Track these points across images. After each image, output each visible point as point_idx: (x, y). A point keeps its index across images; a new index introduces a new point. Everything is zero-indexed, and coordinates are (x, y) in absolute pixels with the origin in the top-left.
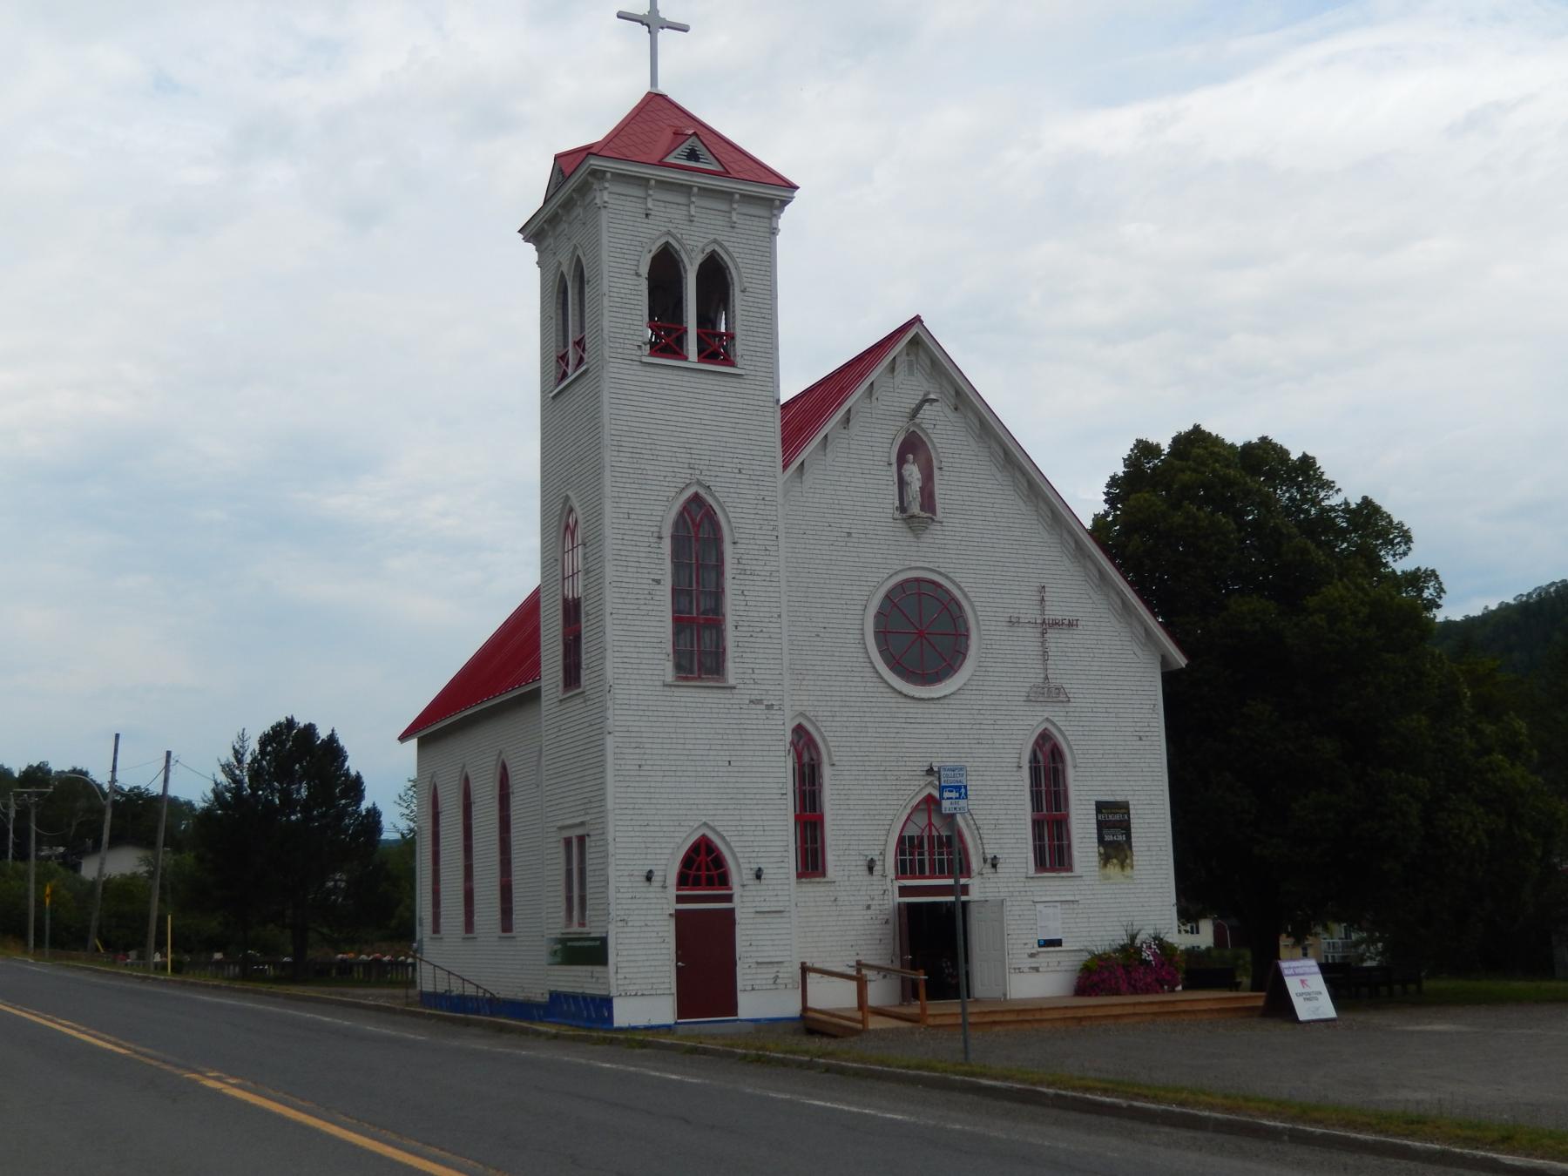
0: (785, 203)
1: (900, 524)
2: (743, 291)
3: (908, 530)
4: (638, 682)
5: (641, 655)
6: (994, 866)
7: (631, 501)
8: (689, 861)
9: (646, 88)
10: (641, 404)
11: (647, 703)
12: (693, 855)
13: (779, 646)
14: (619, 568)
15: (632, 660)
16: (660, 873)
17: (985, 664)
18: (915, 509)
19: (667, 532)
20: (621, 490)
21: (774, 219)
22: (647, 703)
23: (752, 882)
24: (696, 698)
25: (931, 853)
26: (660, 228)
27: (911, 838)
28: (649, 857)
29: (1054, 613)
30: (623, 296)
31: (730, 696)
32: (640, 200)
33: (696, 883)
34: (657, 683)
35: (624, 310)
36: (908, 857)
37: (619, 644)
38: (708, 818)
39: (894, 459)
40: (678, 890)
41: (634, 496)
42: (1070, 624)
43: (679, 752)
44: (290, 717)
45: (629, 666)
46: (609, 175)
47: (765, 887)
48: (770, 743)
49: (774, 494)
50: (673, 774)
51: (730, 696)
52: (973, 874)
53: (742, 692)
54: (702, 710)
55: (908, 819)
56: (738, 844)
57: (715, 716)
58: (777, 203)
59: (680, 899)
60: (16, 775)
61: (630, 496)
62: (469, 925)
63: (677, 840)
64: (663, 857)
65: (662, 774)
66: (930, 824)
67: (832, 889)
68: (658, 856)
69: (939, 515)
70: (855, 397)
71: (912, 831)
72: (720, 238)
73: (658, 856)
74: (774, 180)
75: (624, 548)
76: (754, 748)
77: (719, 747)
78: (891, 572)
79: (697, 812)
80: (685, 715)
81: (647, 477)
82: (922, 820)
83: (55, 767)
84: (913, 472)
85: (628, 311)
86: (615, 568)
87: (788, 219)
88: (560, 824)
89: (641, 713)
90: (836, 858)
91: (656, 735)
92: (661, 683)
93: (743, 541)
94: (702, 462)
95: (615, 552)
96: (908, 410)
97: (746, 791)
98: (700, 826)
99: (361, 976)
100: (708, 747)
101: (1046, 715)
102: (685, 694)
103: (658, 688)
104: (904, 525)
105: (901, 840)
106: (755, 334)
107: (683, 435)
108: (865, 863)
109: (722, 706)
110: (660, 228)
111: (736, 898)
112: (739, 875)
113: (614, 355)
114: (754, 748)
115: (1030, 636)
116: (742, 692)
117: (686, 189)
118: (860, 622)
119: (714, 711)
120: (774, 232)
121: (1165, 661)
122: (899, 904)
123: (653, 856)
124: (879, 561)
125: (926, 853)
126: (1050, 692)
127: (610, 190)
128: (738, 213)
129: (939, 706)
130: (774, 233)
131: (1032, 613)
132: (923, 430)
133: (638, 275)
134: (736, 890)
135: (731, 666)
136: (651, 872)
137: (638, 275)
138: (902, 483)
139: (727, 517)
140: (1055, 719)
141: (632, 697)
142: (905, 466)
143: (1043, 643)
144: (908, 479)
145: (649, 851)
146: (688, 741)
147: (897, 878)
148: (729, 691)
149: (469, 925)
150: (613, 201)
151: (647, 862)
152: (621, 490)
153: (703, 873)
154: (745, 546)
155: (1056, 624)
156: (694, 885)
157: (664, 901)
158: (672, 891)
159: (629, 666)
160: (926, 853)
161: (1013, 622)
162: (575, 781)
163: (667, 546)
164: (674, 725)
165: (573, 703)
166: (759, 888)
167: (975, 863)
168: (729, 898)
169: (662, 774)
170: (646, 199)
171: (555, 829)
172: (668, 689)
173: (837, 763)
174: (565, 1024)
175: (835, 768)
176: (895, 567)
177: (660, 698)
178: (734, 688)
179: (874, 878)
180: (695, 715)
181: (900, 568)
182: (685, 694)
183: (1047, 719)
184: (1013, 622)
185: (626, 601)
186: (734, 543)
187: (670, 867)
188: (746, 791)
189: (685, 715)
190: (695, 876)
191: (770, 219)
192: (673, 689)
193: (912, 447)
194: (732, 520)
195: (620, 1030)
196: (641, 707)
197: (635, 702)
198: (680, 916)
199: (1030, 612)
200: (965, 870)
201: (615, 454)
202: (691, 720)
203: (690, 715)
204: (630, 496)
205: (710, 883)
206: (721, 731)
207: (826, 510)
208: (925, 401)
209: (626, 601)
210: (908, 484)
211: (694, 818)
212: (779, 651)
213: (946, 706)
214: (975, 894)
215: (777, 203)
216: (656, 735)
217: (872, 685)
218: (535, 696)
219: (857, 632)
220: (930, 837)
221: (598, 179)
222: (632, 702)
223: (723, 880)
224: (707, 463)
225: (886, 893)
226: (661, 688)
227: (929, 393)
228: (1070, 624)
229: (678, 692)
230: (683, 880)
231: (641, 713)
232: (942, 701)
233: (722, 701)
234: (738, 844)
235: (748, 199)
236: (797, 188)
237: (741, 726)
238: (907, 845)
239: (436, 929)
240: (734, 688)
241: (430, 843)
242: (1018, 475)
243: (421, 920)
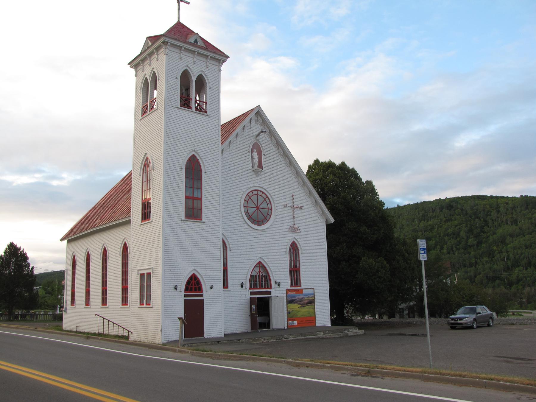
0: (224, 61)
1: (252, 172)
2: (210, 89)
3: (254, 174)
4: (173, 219)
5: (174, 209)
6: (279, 285)
7: (172, 155)
8: (188, 283)
9: (176, 21)
10: (177, 122)
11: (176, 226)
12: (190, 280)
13: (219, 209)
14: (168, 178)
15: (171, 211)
16: (180, 287)
17: (277, 219)
18: (256, 167)
19: (184, 167)
20: (169, 151)
21: (220, 66)
22: (176, 226)
23: (209, 290)
24: (192, 224)
25: (259, 281)
26: (184, 64)
27: (253, 276)
28: (176, 280)
29: (296, 204)
30: (172, 85)
31: (203, 225)
32: (178, 54)
33: (191, 290)
34: (179, 219)
35: (172, 90)
36: (252, 282)
37: (167, 205)
38: (195, 267)
39: (250, 151)
40: (185, 292)
41: (173, 153)
42: (301, 208)
43: (186, 244)
44: (378, 194)
45: (170, 213)
46: (169, 44)
47: (213, 292)
48: (216, 242)
49: (218, 157)
50: (184, 252)
51: (203, 225)
52: (272, 288)
53: (207, 224)
54: (194, 230)
55: (253, 269)
56: (205, 277)
57: (198, 232)
58: (222, 61)
59: (186, 296)
60: (385, 208)
61: (172, 153)
62: (87, 303)
63: (185, 275)
64: (180, 281)
65: (180, 251)
66: (260, 271)
67: (230, 292)
68: (179, 281)
69: (264, 170)
70: (239, 129)
71: (254, 273)
72: (203, 70)
73: (179, 281)
74: (223, 54)
75: (170, 171)
76: (210, 243)
77: (199, 243)
78: (249, 187)
79: (192, 265)
80: (188, 231)
81: (178, 147)
82: (257, 270)
83: (448, 198)
84: (256, 155)
85: (173, 90)
86: (166, 178)
87: (224, 67)
88: (139, 268)
89: (174, 230)
90: (231, 282)
91: (179, 238)
92: (180, 219)
93: (208, 172)
94: (196, 144)
95: (166, 172)
96: (255, 135)
97: (208, 258)
98: (192, 271)
99: (29, 318)
100: (196, 243)
101: (294, 236)
102: (188, 224)
103: (180, 221)
104: (253, 172)
105: (251, 275)
106: (213, 103)
107: (190, 134)
108: (240, 284)
109: (200, 228)
110: (184, 64)
111: (204, 296)
112: (205, 287)
113: (168, 105)
114: (210, 243)
115: (290, 210)
116: (207, 224)
117: (193, 52)
118: (239, 201)
119: (198, 230)
120: (220, 71)
121: (327, 220)
122: (250, 297)
123: (177, 281)
124: (246, 183)
125: (258, 281)
126: (295, 229)
127: (169, 49)
128: (209, 63)
129: (263, 232)
130: (220, 71)
131: (290, 204)
132: (259, 142)
133: (177, 78)
134: (204, 293)
135: (203, 215)
136: (176, 286)
137: (177, 78)
138: (253, 158)
139: (204, 165)
140: (296, 238)
141: (171, 224)
142: (253, 153)
143: (293, 213)
144: (254, 157)
145: (176, 279)
146: (189, 240)
147: (250, 289)
148: (202, 223)
149: (87, 303)
150: (170, 53)
151: (175, 282)
152: (169, 151)
153: (190, 286)
154: (209, 174)
155: (297, 207)
156: (190, 291)
157: (180, 296)
158: (183, 293)
159: (170, 213)
160: (258, 281)
161: (285, 206)
162: (145, 254)
163: (184, 171)
164: (184, 234)
165: (146, 226)
166: (211, 292)
167: (273, 284)
168: (201, 296)
169: (180, 251)
170: (180, 54)
171: (137, 270)
172: (183, 222)
173: (232, 250)
174: (157, 344)
175: (231, 252)
176: (250, 186)
177: (180, 225)
178: (204, 222)
179: (243, 289)
180: (192, 231)
181: (252, 186)
182: (188, 224)
183: (294, 238)
184: (285, 206)
185: (170, 190)
186: (205, 173)
187: (182, 286)
188: (208, 258)
189: (188, 231)
190: (198, 287)
191: (219, 66)
192: (185, 222)
193: (257, 148)
194: (205, 165)
195: (273, 330)
196: (174, 228)
197: (172, 226)
198: (185, 301)
199: (290, 204)
200: (269, 286)
201: (168, 138)
202: (190, 233)
203: (190, 231)
204: (172, 153)
205: (196, 290)
206: (200, 237)
207: (230, 165)
208: (262, 132)
209: (170, 190)
210: (254, 159)
211: (191, 267)
212: (219, 211)
213: (265, 232)
214: (273, 294)
215: (222, 61)
216: (179, 238)
217: (243, 224)
218: (129, 222)
219: (239, 205)
220: (259, 276)
221: (165, 45)
222: (171, 226)
223: (200, 289)
224: (197, 144)
225: (246, 294)
226: (181, 221)
227: (263, 129)
228: (301, 208)
229: (187, 223)
230: (187, 289)
231: (174, 230)
232: (264, 231)
233: (200, 227)
234: (205, 277)
235: (213, 58)
236: (228, 57)
237: (206, 236)
238: (253, 278)
239: (73, 303)
240: (204, 222)
241: (71, 275)
242: (287, 158)
243: (66, 301)
